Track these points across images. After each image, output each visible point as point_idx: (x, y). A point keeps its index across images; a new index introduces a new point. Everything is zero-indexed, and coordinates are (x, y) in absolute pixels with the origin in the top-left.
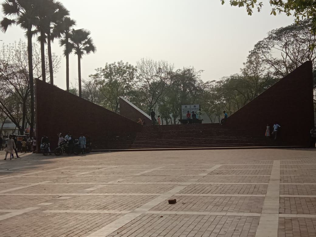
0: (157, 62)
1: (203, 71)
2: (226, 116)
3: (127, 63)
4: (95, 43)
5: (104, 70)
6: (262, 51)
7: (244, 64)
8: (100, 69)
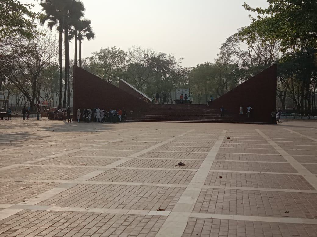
0: (146, 49)
1: (183, 59)
2: (212, 100)
3: (120, 49)
4: (94, 30)
5: (99, 54)
6: (232, 44)
7: (218, 55)
8: (95, 53)
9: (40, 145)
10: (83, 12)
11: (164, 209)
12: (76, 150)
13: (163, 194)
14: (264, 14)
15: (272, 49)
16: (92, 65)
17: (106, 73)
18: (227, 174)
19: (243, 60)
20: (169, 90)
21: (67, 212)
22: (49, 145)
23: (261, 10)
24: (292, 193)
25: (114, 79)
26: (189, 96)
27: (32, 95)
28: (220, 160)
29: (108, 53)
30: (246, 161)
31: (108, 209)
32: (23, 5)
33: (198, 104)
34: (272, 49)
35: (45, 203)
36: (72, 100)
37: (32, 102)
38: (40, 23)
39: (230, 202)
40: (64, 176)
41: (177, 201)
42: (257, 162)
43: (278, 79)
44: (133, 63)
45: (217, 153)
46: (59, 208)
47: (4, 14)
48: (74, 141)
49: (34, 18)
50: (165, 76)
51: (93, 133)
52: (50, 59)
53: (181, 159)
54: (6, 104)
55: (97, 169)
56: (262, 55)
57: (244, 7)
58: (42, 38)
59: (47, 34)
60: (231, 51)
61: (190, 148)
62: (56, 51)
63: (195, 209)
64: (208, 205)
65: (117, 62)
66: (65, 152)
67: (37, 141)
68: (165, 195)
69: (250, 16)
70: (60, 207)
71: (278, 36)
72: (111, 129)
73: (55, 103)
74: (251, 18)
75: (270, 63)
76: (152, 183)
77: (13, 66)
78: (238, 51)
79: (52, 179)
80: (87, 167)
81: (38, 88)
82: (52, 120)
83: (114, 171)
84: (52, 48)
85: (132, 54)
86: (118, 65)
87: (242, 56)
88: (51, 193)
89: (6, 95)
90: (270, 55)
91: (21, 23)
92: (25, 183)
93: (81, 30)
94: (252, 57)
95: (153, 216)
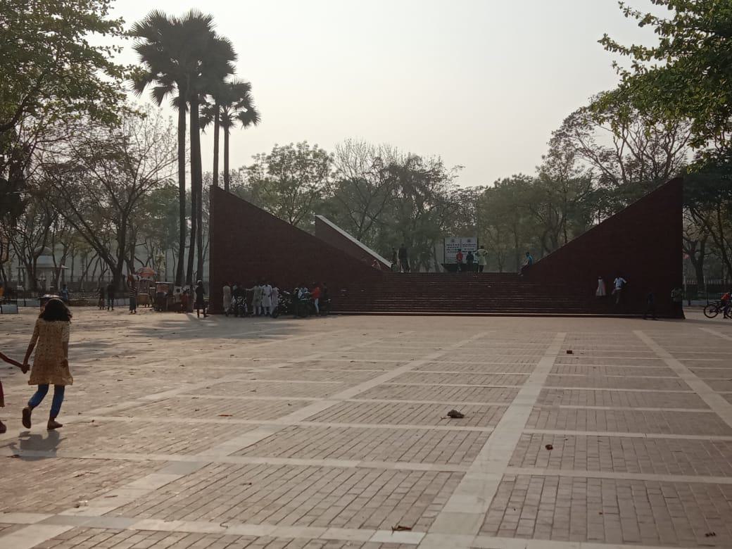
3: (316, 146)
4: (257, 104)
5: (269, 158)
6: (577, 132)
7: (543, 157)
8: (261, 156)
9: (128, 369)
10: (232, 63)
11: (408, 527)
12: (210, 383)
13: (407, 490)
14: (649, 60)
15: (670, 142)
16: (254, 185)
17: (286, 202)
18: (565, 439)
19: (602, 168)
20: (429, 241)
21: (176, 534)
22: (149, 371)
23: (643, 50)
24: (722, 485)
25: (304, 215)
26: (477, 254)
27: (117, 255)
28: (548, 406)
29: (290, 157)
30: (613, 408)
31: (276, 527)
32: (95, 48)
33: (499, 272)
34: (670, 142)
35: (126, 510)
36: (206, 265)
37: (117, 271)
38: (135, 88)
39: (570, 508)
40: (178, 444)
41: (442, 506)
42: (637, 409)
43: (686, 212)
44: (347, 178)
45: (541, 387)
46: (158, 524)
47: (52, 69)
48: (208, 361)
49: (120, 77)
50: (421, 207)
51: (252, 341)
52: (158, 172)
53: (456, 403)
54: (58, 276)
55: (256, 427)
56: (647, 156)
57: (604, 44)
58: (140, 123)
59: (152, 115)
60: (574, 149)
61: (478, 375)
62: (172, 155)
63: (486, 527)
64: (518, 517)
65: (310, 176)
66: (185, 387)
67: (123, 360)
68: (412, 492)
69: (615, 65)
70: (161, 522)
71: (684, 111)
72: (295, 332)
73: (170, 274)
74: (619, 69)
75: (666, 175)
76: (384, 461)
77: (75, 189)
78: (591, 149)
79: (148, 451)
80: (232, 421)
81: (131, 239)
82: (160, 312)
83: (296, 432)
84: (163, 147)
85: (344, 158)
86: (312, 184)
87: (602, 160)
88: (144, 484)
89: (58, 257)
90: (667, 156)
91: (91, 89)
92: (84, 462)
93: (230, 106)
94: (625, 161)
95: (383, 543)
